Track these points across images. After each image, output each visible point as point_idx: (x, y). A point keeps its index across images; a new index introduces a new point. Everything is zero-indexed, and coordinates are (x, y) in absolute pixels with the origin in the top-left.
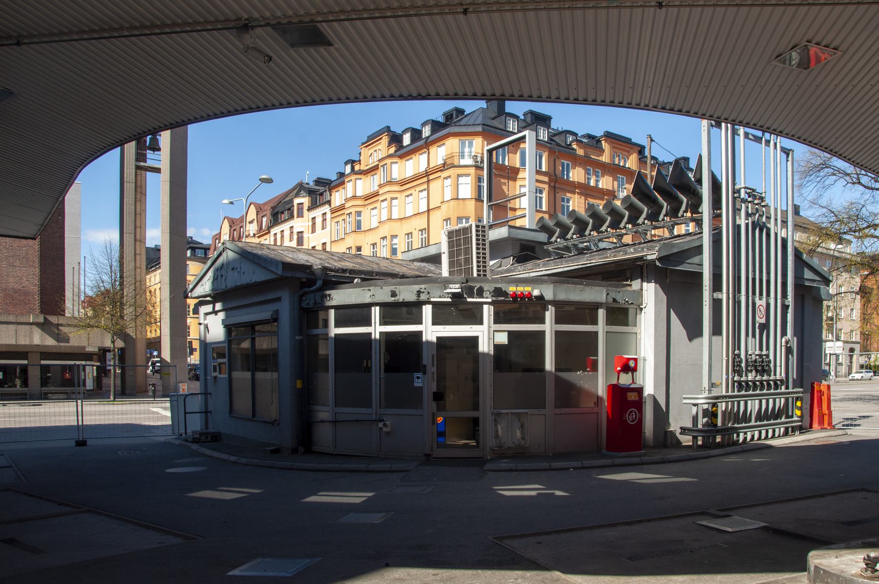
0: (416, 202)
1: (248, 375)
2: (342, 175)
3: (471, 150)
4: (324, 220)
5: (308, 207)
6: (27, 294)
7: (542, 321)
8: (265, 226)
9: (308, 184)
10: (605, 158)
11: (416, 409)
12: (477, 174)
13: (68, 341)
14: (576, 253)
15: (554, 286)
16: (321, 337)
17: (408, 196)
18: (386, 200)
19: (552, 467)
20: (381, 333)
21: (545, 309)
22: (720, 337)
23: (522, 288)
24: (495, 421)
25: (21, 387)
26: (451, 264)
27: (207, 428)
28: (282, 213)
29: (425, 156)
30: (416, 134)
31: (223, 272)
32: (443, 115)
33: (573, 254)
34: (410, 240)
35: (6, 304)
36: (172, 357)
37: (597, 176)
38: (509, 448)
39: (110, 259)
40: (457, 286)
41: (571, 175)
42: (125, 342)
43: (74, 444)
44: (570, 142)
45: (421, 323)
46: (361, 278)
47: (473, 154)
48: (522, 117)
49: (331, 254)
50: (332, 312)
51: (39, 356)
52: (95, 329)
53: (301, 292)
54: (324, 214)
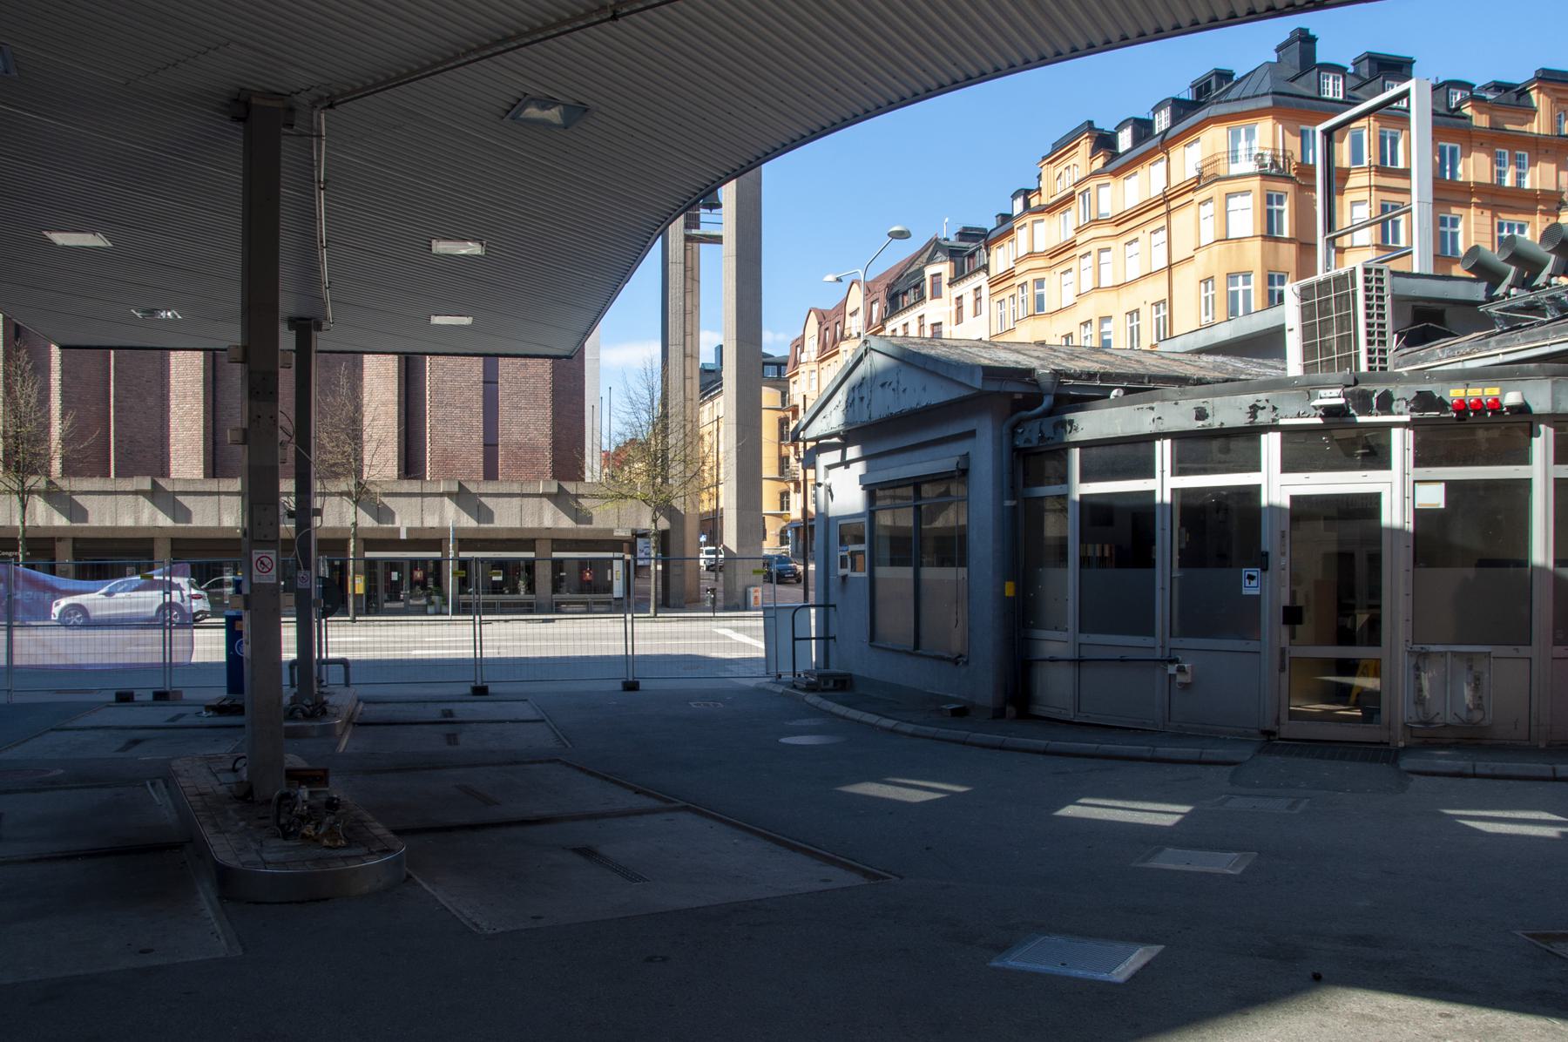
0: (1148, 250)
1: (907, 572)
2: (1006, 218)
3: (1250, 143)
4: (978, 299)
5: (950, 279)
6: (534, 449)
7: (1525, 460)
8: (877, 319)
9: (947, 239)
10: (1538, 126)
11: (1244, 639)
12: (1264, 188)
13: (589, 520)
14: (1557, 316)
15: (1554, 383)
16: (1048, 505)
17: (1129, 243)
18: (1089, 253)
19: (1558, 775)
20: (1173, 490)
21: (1532, 432)
22: (566, 562)
23: (1480, 390)
24: (1417, 668)
25: (526, 593)
26: (1308, 351)
27: (827, 665)
28: (905, 293)
29: (1162, 166)
30: (1142, 128)
31: (865, 392)
32: (1192, 87)
33: (1550, 318)
34: (1135, 323)
35: (508, 466)
36: (739, 545)
37: (1520, 166)
38: (1446, 726)
39: (651, 389)
40: (1336, 392)
41: (1460, 169)
42: (670, 521)
43: (620, 687)
44: (1458, 103)
45: (1257, 468)
46: (1122, 388)
47: (1255, 152)
48: (1351, 70)
49: (1051, 349)
50: (1076, 454)
51: (549, 543)
52: (629, 500)
53: (1015, 418)
54: (978, 289)
